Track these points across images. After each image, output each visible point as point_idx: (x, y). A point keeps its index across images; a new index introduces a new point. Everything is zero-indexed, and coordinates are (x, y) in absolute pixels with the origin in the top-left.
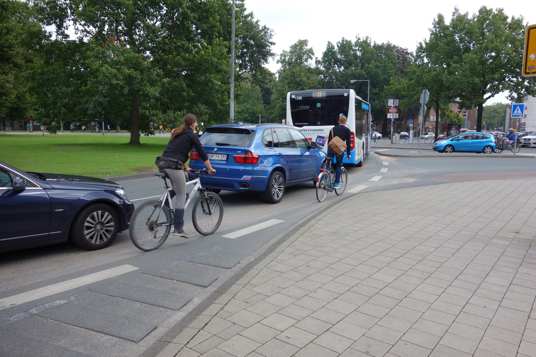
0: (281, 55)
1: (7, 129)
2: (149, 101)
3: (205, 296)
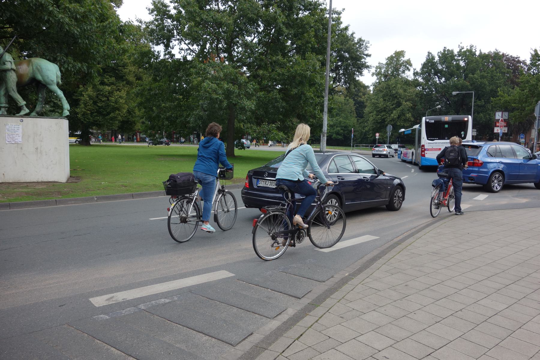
0: (377, 67)
1: (93, 141)
2: (245, 114)
3: (299, 308)
